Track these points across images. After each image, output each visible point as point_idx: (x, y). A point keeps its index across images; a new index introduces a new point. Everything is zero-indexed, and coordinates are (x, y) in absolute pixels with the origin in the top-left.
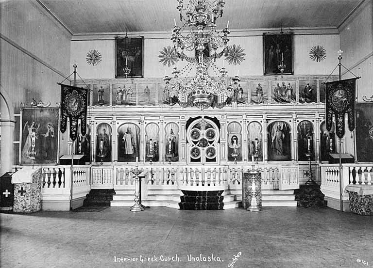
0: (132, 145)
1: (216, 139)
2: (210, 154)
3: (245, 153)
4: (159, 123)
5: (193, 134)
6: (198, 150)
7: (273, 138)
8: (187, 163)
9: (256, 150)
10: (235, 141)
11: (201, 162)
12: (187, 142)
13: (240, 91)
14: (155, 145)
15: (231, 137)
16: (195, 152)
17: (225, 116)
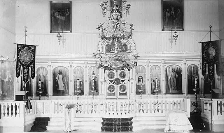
0: (63, 83)
1: (126, 79)
2: (122, 89)
3: (148, 89)
5: (109, 75)
6: (113, 86)
7: (170, 78)
9: (156, 87)
10: (141, 80)
11: (116, 96)
12: (105, 81)
14: (80, 83)
15: (138, 77)
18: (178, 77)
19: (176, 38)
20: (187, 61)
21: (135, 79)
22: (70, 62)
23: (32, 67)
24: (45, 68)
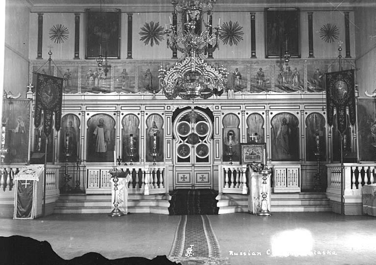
1: (209, 134)
2: (201, 152)
4: (263, 113)
8: (173, 163)
12: (174, 138)
13: (238, 77)
15: (227, 132)
16: (184, 150)
17: (220, 106)
18: (291, 132)
19: (287, 60)
20: (306, 107)
21: (222, 135)
22: (117, 106)
23: (57, 112)
24: (75, 115)
